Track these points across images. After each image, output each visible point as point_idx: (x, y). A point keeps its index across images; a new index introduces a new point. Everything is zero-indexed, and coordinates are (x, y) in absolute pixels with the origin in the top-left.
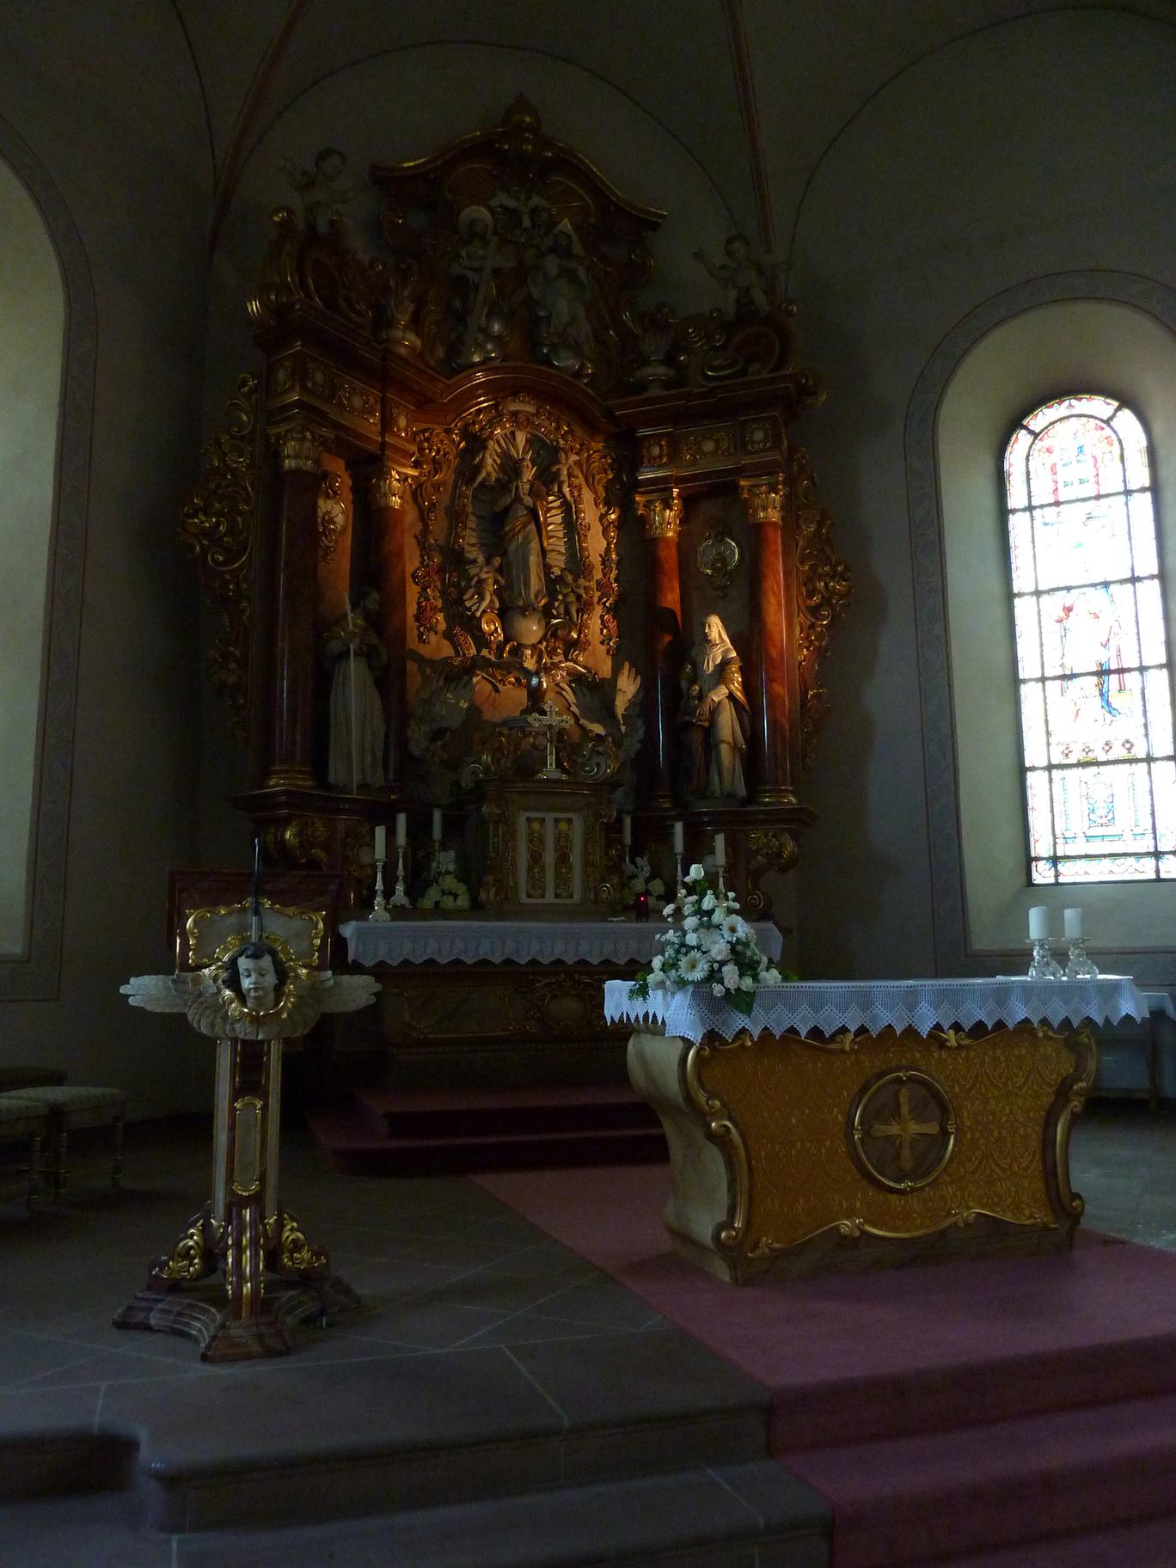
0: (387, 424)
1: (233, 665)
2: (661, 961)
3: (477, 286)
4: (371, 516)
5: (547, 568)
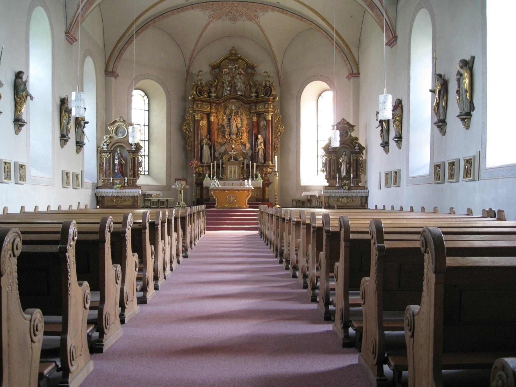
1: (190, 147)
3: (225, 83)
4: (209, 123)
5: (237, 126)
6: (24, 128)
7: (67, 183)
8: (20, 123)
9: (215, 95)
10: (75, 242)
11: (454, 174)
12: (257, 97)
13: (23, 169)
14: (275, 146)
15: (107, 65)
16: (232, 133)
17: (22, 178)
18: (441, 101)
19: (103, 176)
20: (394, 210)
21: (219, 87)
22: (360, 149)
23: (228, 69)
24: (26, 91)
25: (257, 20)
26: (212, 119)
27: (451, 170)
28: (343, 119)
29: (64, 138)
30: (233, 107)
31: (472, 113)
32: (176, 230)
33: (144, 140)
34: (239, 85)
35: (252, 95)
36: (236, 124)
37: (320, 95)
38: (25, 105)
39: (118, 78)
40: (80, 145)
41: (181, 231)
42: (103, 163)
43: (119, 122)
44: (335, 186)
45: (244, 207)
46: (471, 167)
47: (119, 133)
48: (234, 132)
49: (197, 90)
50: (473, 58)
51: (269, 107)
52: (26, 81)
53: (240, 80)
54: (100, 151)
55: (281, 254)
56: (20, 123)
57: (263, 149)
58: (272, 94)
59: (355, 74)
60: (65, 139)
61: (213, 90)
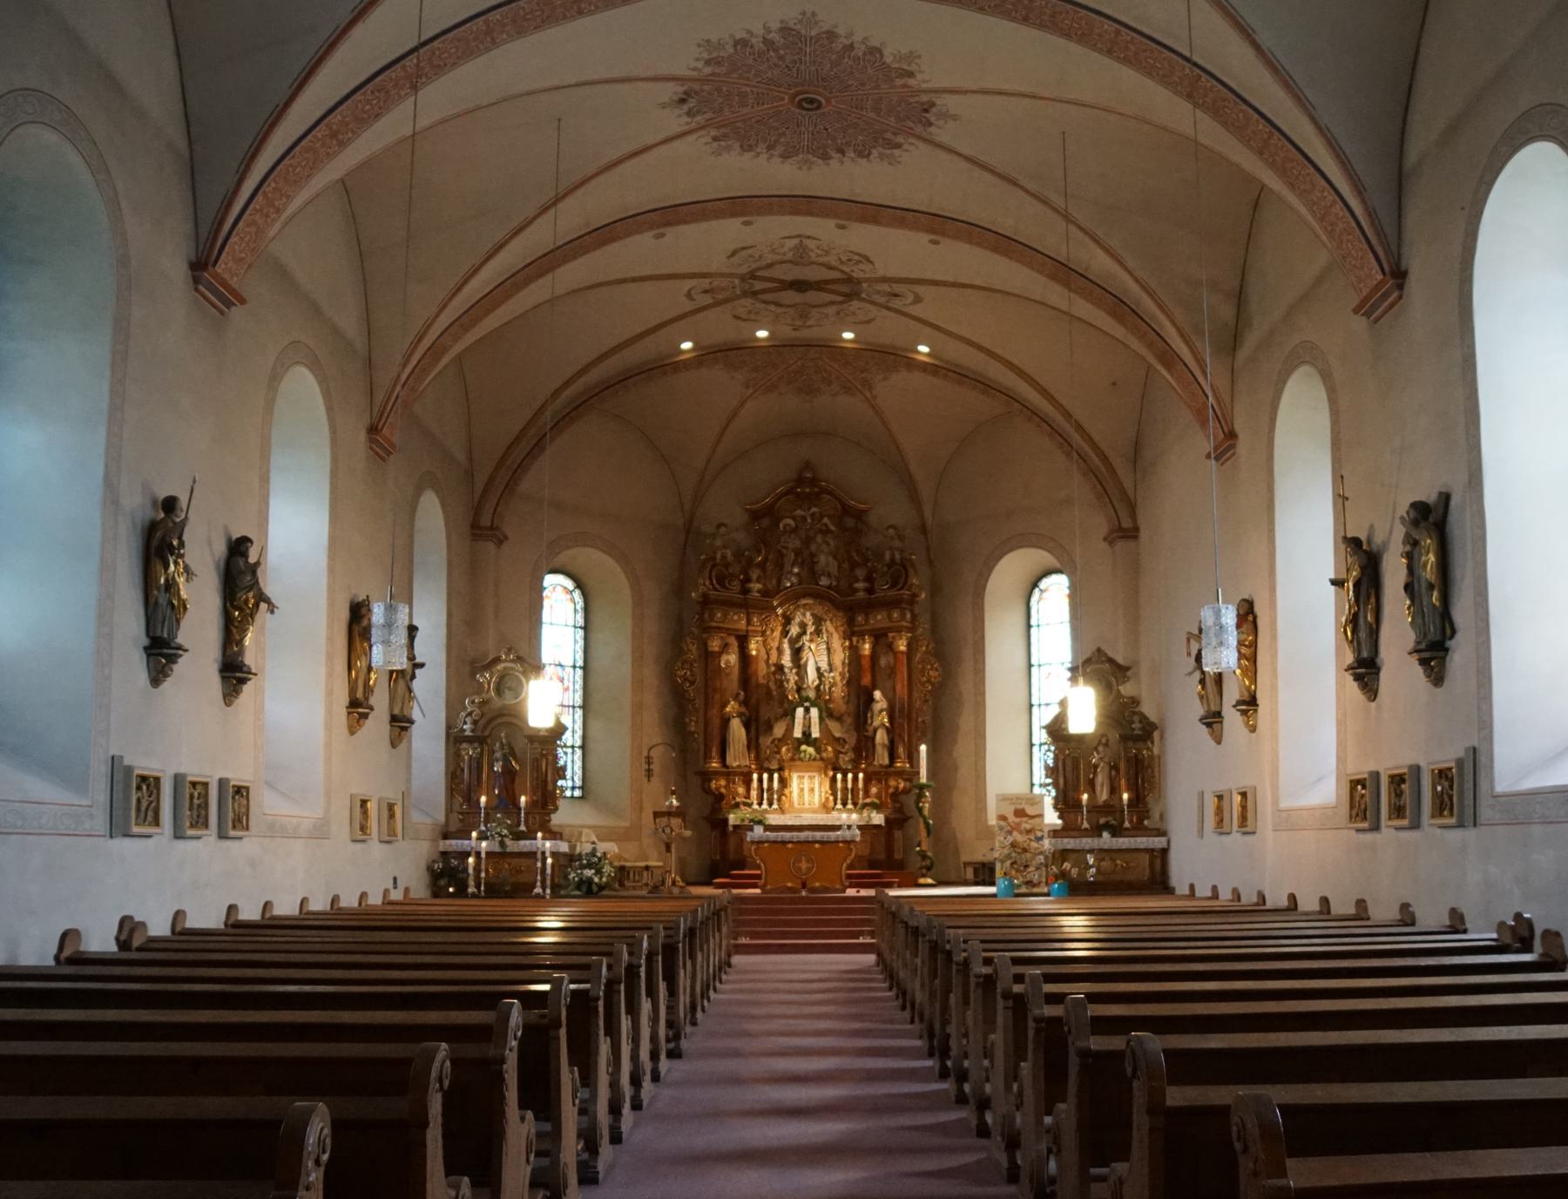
0: (749, 623)
2: (177, 516)
4: (745, 658)
6: (247, 688)
7: (363, 828)
8: (238, 675)
9: (758, 586)
10: (322, 1169)
11: (1404, 807)
12: (870, 591)
13: (242, 796)
14: (920, 720)
15: (477, 510)
16: (805, 686)
17: (240, 821)
18: (1362, 610)
19: (461, 805)
20: (1239, 900)
21: (769, 566)
22: (1142, 729)
23: (794, 518)
24: (255, 589)
25: (868, 395)
26: (754, 648)
27: (1396, 795)
28: (1099, 650)
29: (358, 707)
30: (809, 619)
31: (1449, 644)
32: (652, 993)
33: (571, 704)
34: (822, 559)
35: (856, 585)
36: (816, 663)
37: (1035, 585)
38: (251, 628)
39: (505, 546)
40: (400, 723)
41: (662, 987)
42: (463, 770)
43: (506, 661)
44: (1079, 829)
45: (838, 886)
46: (1452, 789)
47: (506, 690)
48: (810, 682)
49: (714, 574)
50: (1446, 498)
51: (903, 616)
52: (258, 564)
53: (824, 547)
54: (454, 739)
55: (944, 1053)
56: (238, 675)
57: (887, 728)
58: (909, 583)
59: (1125, 532)
60: (360, 710)
61: (755, 574)
